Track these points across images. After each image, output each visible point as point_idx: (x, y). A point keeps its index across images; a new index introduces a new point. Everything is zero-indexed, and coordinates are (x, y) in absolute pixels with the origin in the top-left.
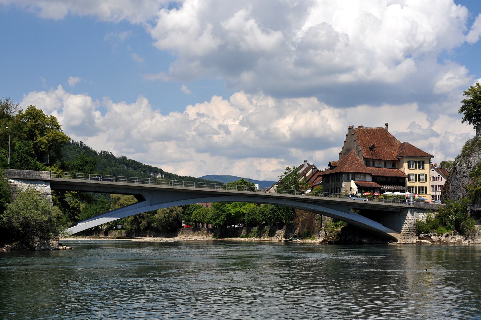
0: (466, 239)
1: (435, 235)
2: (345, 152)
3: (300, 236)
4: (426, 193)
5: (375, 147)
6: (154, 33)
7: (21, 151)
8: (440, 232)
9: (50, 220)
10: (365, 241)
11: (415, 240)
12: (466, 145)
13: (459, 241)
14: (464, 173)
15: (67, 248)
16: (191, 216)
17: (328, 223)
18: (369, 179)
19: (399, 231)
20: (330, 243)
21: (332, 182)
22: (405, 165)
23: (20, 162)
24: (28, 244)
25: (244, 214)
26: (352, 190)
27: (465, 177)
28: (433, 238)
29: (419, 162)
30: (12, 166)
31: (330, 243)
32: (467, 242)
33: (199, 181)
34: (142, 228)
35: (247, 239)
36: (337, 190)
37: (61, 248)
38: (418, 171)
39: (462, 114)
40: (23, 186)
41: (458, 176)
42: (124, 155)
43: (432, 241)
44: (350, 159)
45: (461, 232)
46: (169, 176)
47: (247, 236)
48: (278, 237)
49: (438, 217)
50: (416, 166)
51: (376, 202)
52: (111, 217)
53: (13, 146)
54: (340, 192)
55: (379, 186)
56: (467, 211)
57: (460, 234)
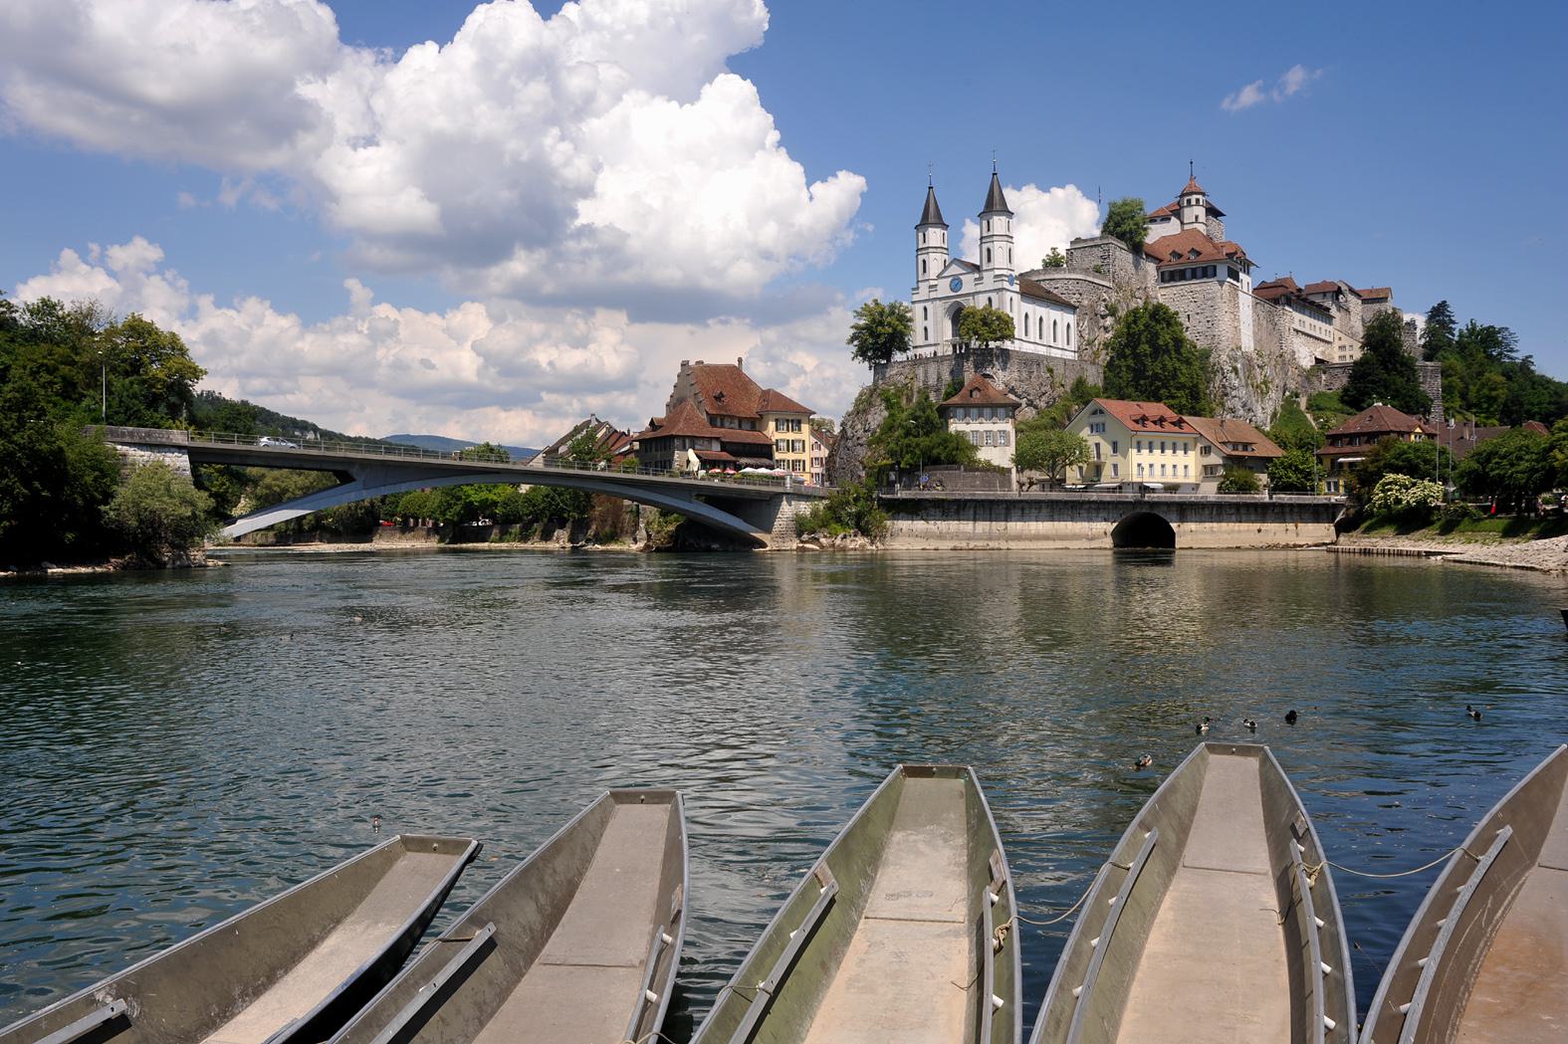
0: (872, 543)
1: (825, 537)
2: (676, 404)
3: (598, 539)
4: (804, 470)
5: (723, 396)
6: (1404, 360)
7: (125, 394)
8: (833, 531)
9: (194, 516)
10: (715, 546)
11: (795, 544)
12: (861, 395)
13: (863, 546)
14: (858, 438)
15: (220, 563)
16: (397, 506)
17: (651, 518)
18: (716, 447)
19: (768, 531)
20: (658, 550)
21: (656, 450)
22: (772, 425)
23: (125, 413)
24: (151, 557)
25: (495, 504)
26: (691, 465)
27: (862, 445)
28: (823, 540)
29: (792, 421)
30: (110, 421)
31: (658, 550)
32: (874, 548)
33: (387, 445)
34: (306, 527)
35: (504, 546)
36: (666, 464)
37: (210, 564)
38: (791, 436)
39: (851, 346)
40: (139, 456)
41: (850, 444)
42: (245, 399)
43: (822, 547)
44: (685, 414)
45: (865, 532)
46: (328, 435)
47: (501, 540)
48: (558, 541)
49: (829, 508)
50: (788, 427)
51: (729, 484)
52: (291, 508)
53: (109, 384)
54: (671, 467)
55: (733, 458)
56: (873, 500)
57: (863, 534)
